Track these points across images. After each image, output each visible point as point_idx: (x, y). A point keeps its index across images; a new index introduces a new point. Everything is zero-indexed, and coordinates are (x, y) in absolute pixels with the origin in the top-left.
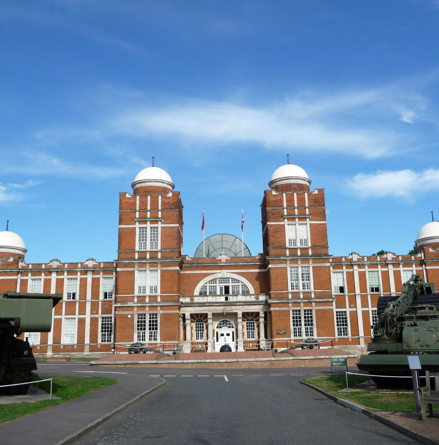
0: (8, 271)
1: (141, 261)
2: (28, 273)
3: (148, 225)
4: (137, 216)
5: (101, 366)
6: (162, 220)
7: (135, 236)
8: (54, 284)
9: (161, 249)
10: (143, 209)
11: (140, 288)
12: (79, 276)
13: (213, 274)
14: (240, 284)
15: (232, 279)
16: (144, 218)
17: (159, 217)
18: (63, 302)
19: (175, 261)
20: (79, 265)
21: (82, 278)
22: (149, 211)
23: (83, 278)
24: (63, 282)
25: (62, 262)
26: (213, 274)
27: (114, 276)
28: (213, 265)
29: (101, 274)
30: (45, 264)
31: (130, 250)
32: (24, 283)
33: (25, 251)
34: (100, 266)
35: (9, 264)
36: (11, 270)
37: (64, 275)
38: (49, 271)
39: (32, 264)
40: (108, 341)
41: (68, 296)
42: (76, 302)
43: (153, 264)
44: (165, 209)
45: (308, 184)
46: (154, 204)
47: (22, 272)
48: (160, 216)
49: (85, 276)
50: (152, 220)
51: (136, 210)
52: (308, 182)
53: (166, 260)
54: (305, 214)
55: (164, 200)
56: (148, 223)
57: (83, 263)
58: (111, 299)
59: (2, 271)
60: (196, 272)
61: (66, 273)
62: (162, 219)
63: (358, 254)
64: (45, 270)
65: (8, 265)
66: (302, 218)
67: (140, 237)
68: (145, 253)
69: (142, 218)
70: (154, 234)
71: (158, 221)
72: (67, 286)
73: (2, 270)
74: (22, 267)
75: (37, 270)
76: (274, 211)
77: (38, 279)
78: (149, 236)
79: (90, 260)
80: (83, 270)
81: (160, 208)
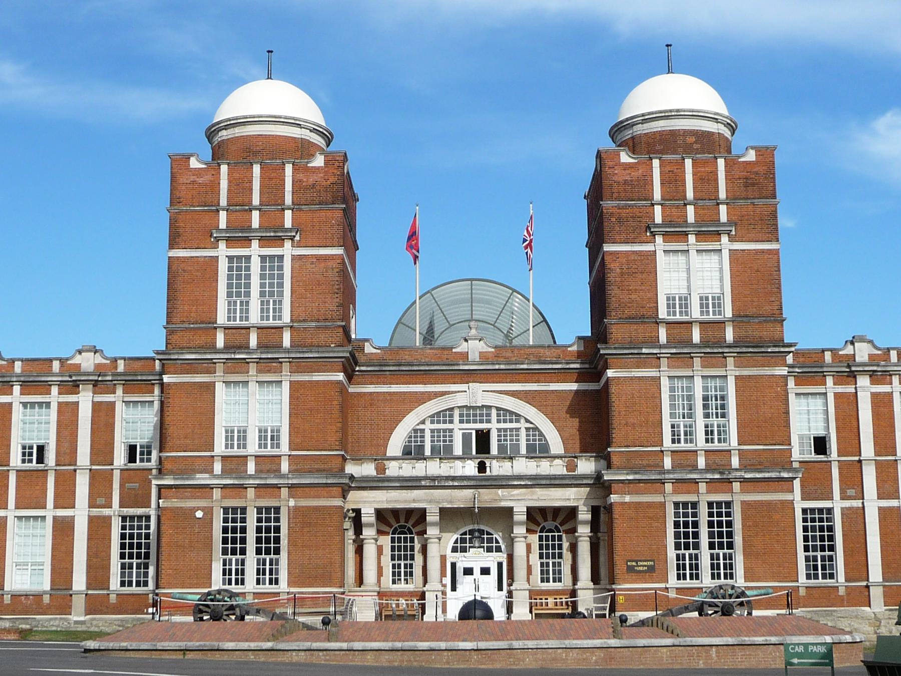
1: (233, 356)
3: (255, 250)
4: (223, 225)
9: (292, 321)
10: (240, 203)
11: (229, 432)
12: (55, 396)
13: (443, 394)
14: (523, 425)
16: (242, 230)
17: (286, 227)
18: (8, 470)
19: (331, 355)
20: (56, 365)
23: (67, 403)
26: (443, 394)
27: (157, 398)
29: (119, 391)
31: (202, 323)
34: (116, 368)
38: (849, 372)
40: (138, 584)
41: (24, 454)
42: (47, 470)
45: (727, 133)
46: (272, 188)
48: (288, 224)
50: (264, 235)
55: (301, 176)
56: (255, 244)
57: (67, 359)
60: (395, 388)
61: (17, 389)
62: (294, 234)
63: (871, 342)
66: (709, 232)
67: (229, 286)
68: (243, 331)
76: (624, 213)
78: (255, 281)
81: (288, 200)
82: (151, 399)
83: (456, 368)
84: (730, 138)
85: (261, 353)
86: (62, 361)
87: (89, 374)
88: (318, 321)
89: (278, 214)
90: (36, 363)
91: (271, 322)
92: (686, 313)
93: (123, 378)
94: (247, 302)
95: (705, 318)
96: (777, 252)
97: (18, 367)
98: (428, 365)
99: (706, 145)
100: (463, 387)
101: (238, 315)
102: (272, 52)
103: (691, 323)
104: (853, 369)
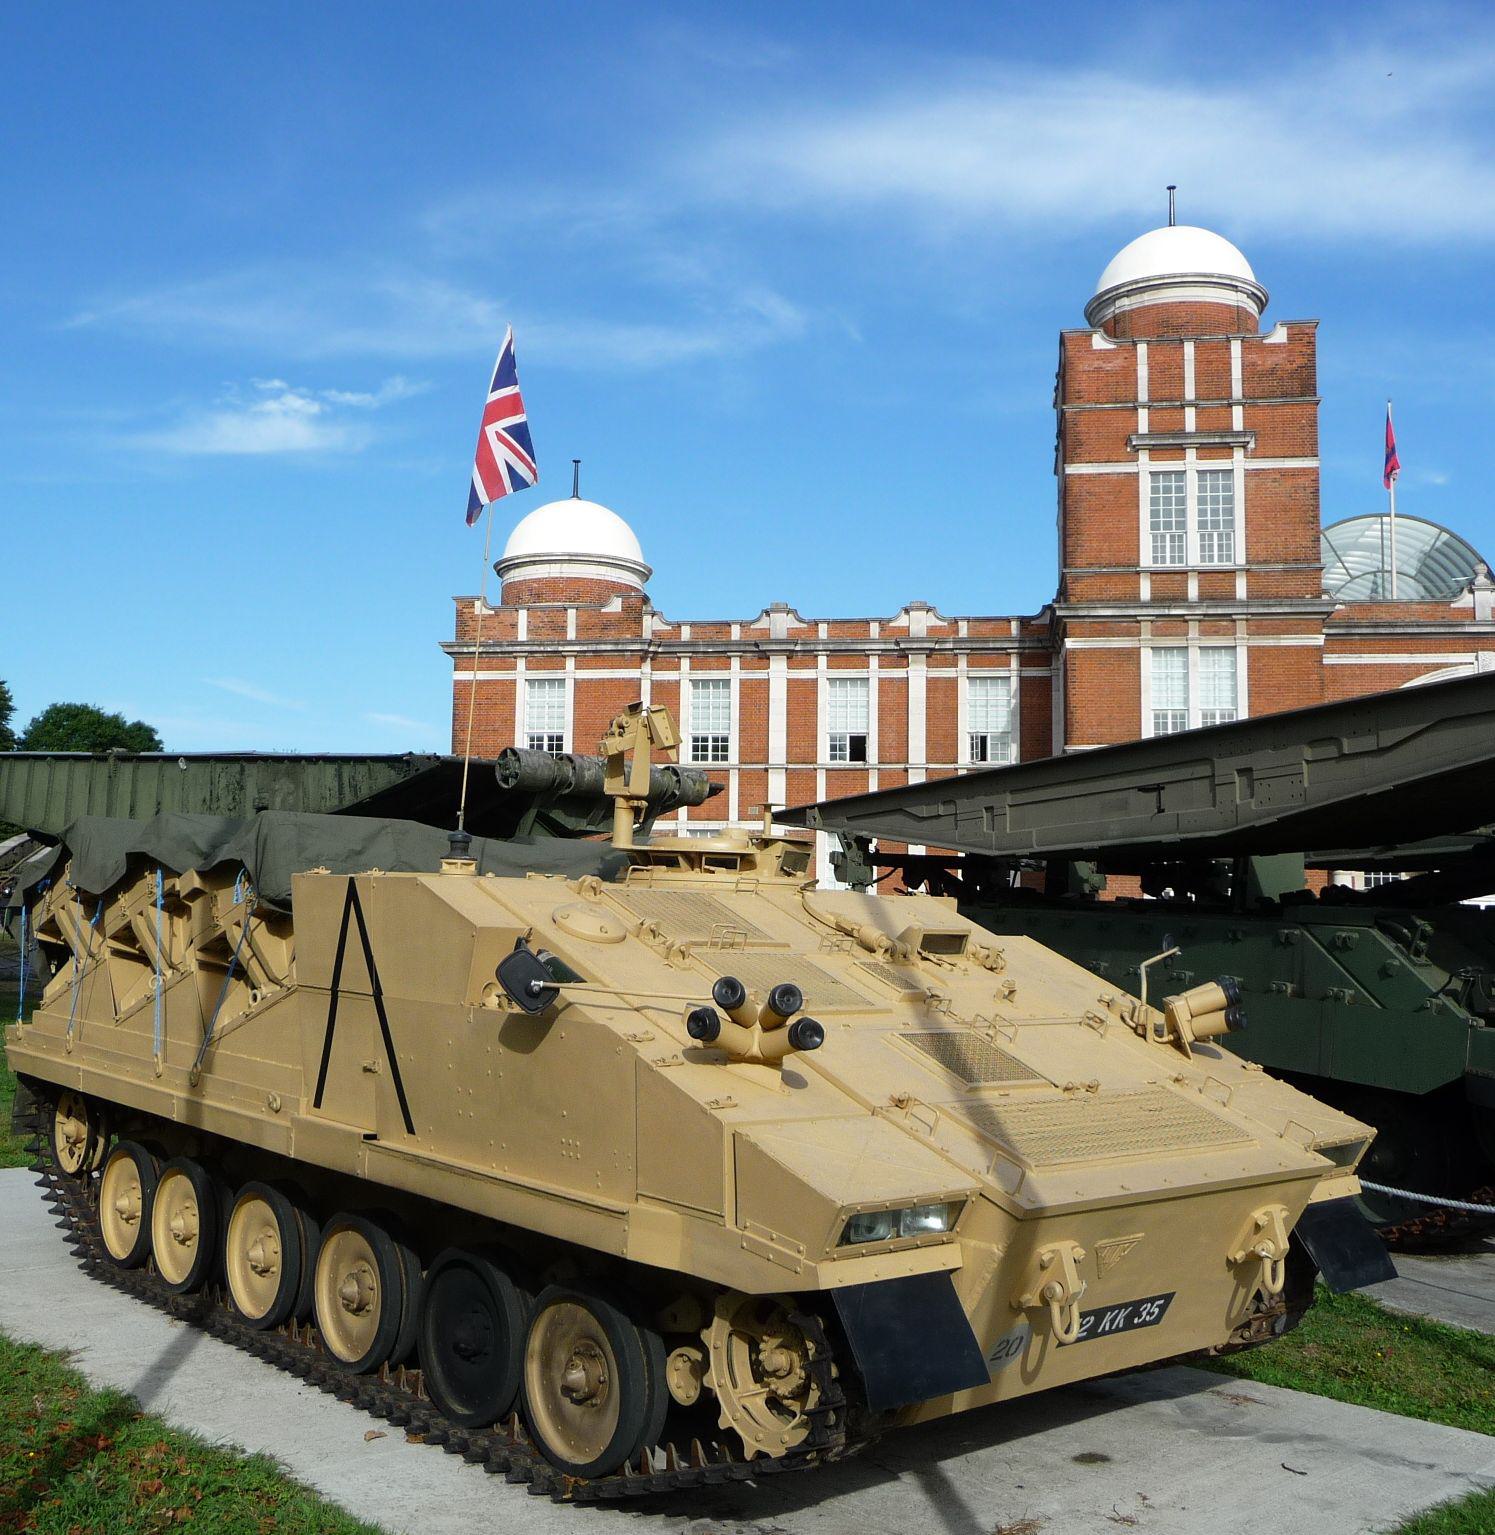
0: (609, 647)
1: (1166, 612)
2: (679, 658)
3: (1191, 462)
4: (1143, 428)
6: (1248, 443)
7: (1138, 506)
8: (781, 700)
9: (1248, 562)
10: (1166, 399)
12: (874, 670)
16: (1175, 435)
17: (1235, 429)
18: (815, 769)
19: (1309, 609)
20: (874, 628)
21: (886, 678)
22: (1144, 407)
23: (891, 680)
24: (816, 693)
25: (941, 612)
27: (1014, 673)
28: (1442, 630)
29: (963, 662)
30: (880, 621)
31: (1118, 565)
33: (645, 575)
34: (957, 632)
35: (607, 624)
36: (620, 647)
37: (678, 668)
38: (759, 653)
39: (693, 625)
41: (695, 749)
42: (868, 770)
43: (1214, 623)
44: (1261, 395)
45: (1252, 307)
46: (1214, 374)
47: (655, 653)
48: (1238, 424)
49: (899, 673)
50: (1205, 441)
51: (1136, 400)
52: (1253, 296)
53: (1275, 606)
54: (1228, 431)
55: (1253, 357)
56: (1191, 454)
57: (890, 620)
58: (725, 762)
59: (585, 648)
60: (1367, 659)
61: (822, 660)
62: (1247, 439)
64: (742, 648)
65: (605, 627)
67: (1154, 514)
68: (1178, 577)
69: (1210, 433)
70: (1215, 500)
71: (1232, 448)
72: (527, 709)
73: (583, 644)
74: (654, 633)
75: (711, 647)
77: (716, 682)
78: (1192, 507)
79: (919, 609)
80: (893, 647)
81: (1237, 391)
82: (1006, 674)
83: (1459, 630)
84: (1257, 315)
85: (1208, 607)
87: (922, 640)
88: (1286, 561)
89: (1223, 413)
90: (847, 626)
91: (1216, 564)
92: (1229, 558)
93: (969, 645)
94: (1180, 537)
95: (1207, 565)
96: (1315, 471)
97: (823, 631)
98: (1418, 626)
99: (1210, 327)
101: (1168, 555)
102: (1173, 188)
103: (1185, 573)
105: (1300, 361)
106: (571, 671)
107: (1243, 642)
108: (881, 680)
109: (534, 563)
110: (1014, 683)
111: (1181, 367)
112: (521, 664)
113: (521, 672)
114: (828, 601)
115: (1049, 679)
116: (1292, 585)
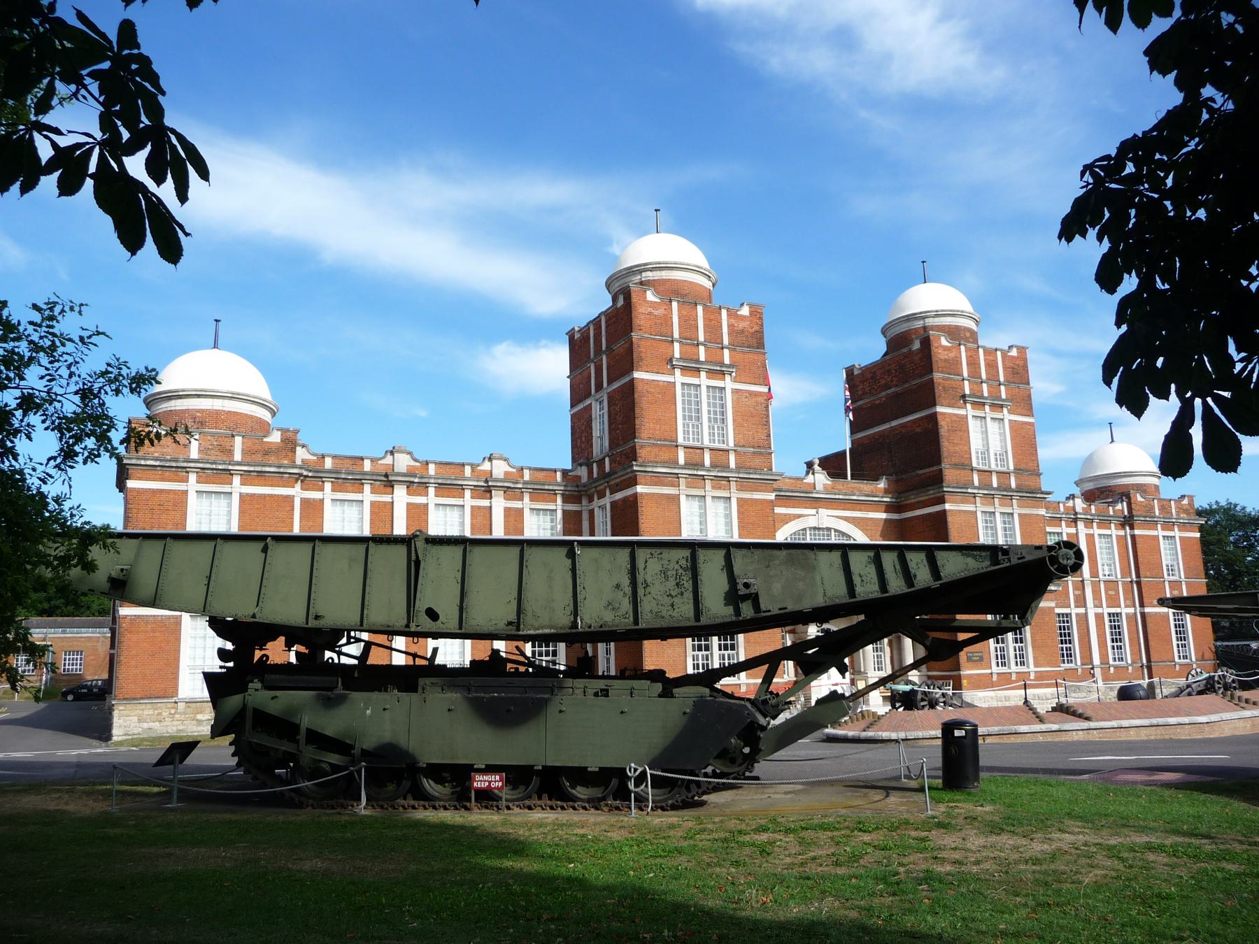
4: (677, 355)
5: (921, 743)
10: (689, 339)
12: (468, 500)
13: (799, 516)
15: (836, 531)
20: (468, 470)
23: (479, 508)
25: (512, 462)
26: (799, 516)
29: (527, 498)
32: (313, 509)
34: (522, 476)
35: (268, 451)
37: (323, 490)
38: (387, 481)
39: (334, 457)
61: (431, 490)
63: (410, 453)
65: (266, 453)
75: (348, 476)
79: (500, 458)
81: (726, 341)
86: (474, 467)
87: (501, 481)
100: (813, 511)
104: (391, 478)
105: (756, 328)
106: (237, 487)
107: (735, 495)
108: (472, 507)
109: (199, 396)
110: (559, 514)
111: (696, 320)
112: (193, 477)
113: (192, 484)
114: (439, 449)
115: (580, 513)
116: (757, 461)
